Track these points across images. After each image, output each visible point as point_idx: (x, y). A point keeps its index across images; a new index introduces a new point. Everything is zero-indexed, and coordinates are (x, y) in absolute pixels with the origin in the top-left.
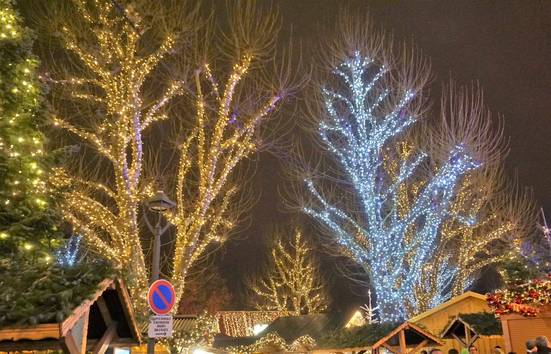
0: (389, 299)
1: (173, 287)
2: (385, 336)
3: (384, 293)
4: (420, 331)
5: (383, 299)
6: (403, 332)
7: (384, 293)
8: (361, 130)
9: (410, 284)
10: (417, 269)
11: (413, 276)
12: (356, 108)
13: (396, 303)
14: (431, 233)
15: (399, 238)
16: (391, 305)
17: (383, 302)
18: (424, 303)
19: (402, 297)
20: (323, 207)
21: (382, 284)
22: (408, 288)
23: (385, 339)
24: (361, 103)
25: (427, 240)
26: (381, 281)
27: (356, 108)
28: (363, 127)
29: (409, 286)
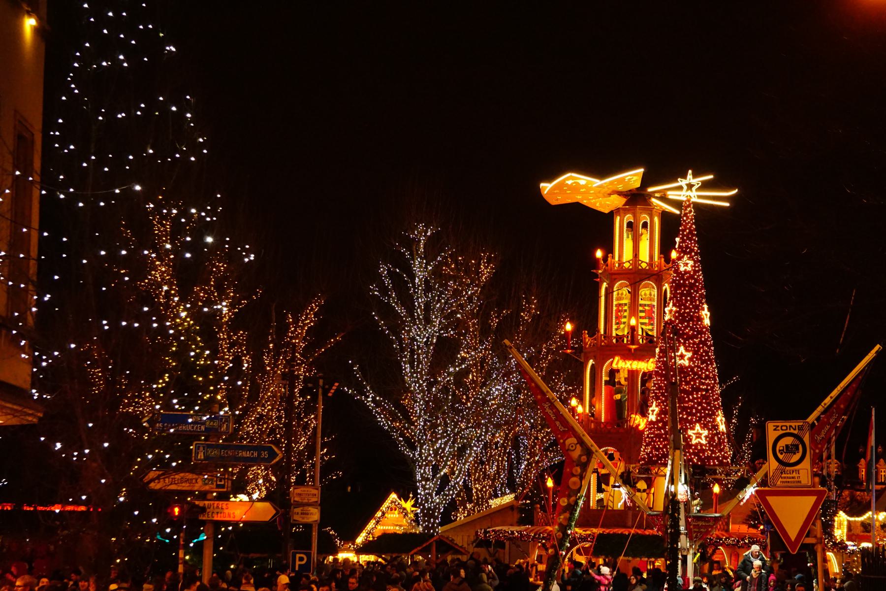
0: (431, 504)
1: (678, 405)
2: (419, 546)
3: (426, 498)
4: (448, 542)
5: (425, 503)
6: (434, 543)
7: (426, 498)
8: (418, 315)
9: (454, 489)
10: (464, 472)
11: (458, 480)
12: (415, 288)
13: (437, 508)
14: (483, 433)
15: (702, 406)
16: (432, 510)
17: (424, 506)
18: (482, 495)
19: (444, 502)
20: (581, 422)
21: (425, 489)
22: (451, 492)
23: (419, 548)
24: (421, 284)
25: (478, 441)
26: (423, 486)
27: (415, 288)
28: (421, 312)
29: (453, 491)
